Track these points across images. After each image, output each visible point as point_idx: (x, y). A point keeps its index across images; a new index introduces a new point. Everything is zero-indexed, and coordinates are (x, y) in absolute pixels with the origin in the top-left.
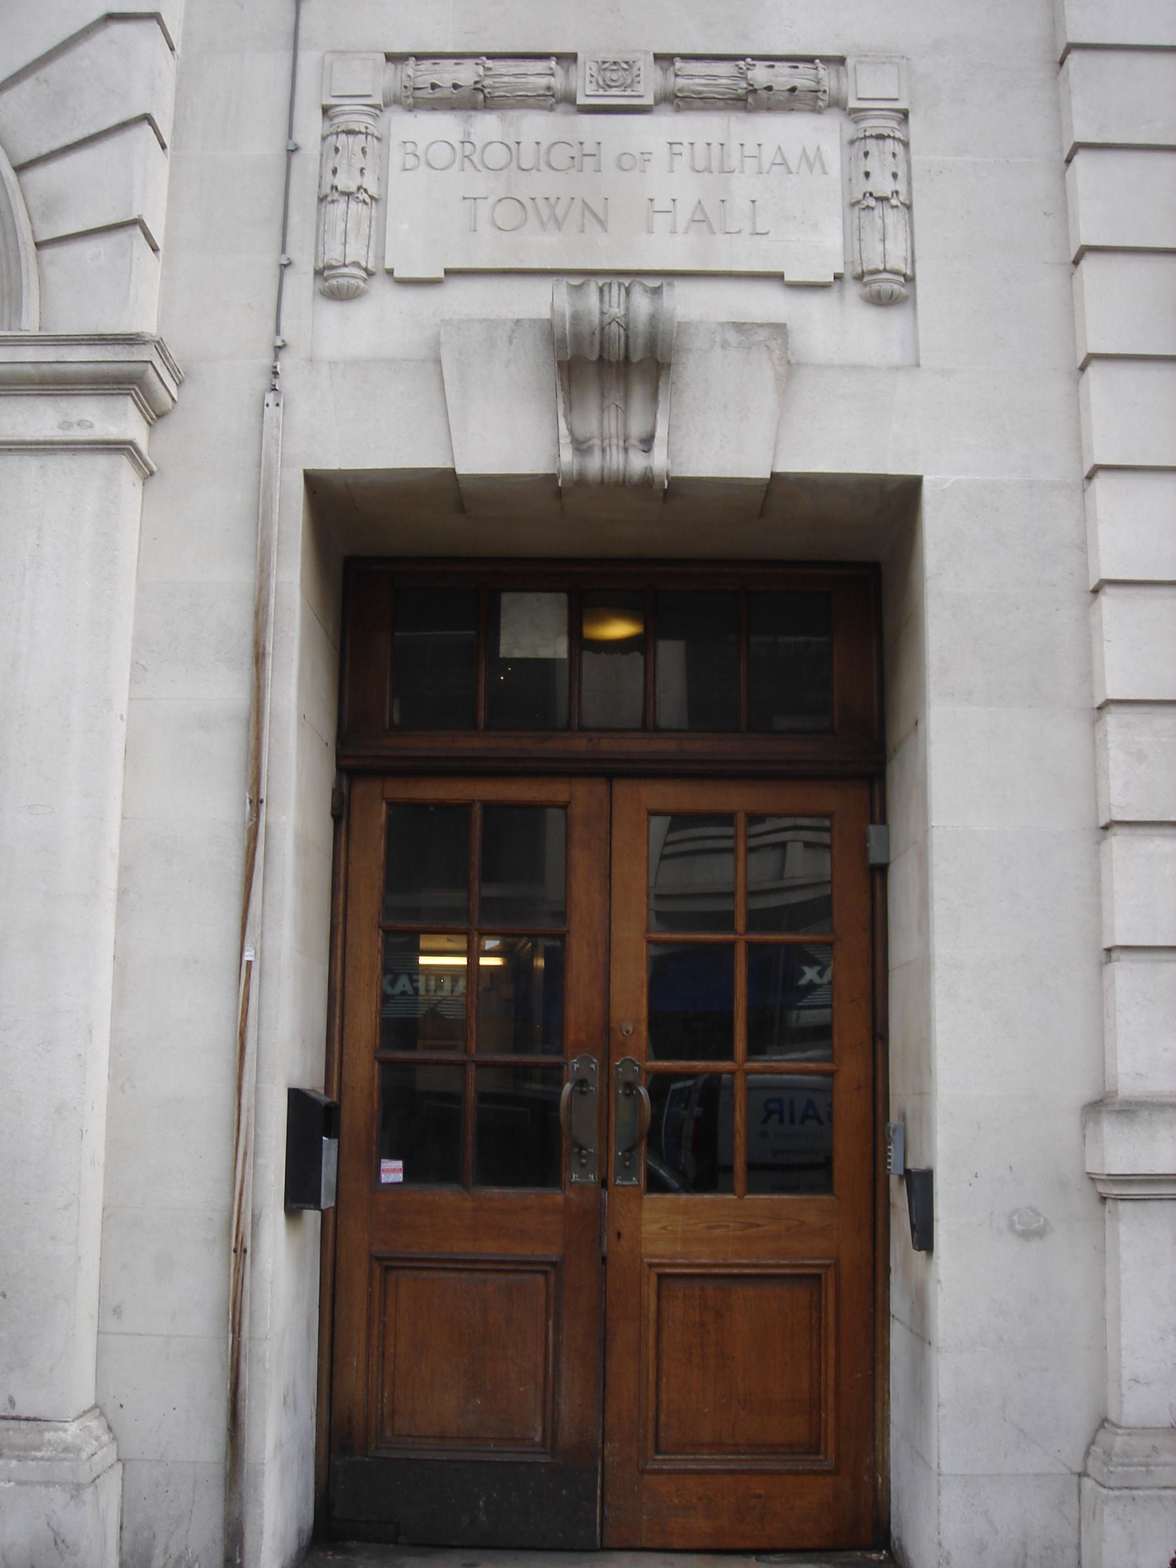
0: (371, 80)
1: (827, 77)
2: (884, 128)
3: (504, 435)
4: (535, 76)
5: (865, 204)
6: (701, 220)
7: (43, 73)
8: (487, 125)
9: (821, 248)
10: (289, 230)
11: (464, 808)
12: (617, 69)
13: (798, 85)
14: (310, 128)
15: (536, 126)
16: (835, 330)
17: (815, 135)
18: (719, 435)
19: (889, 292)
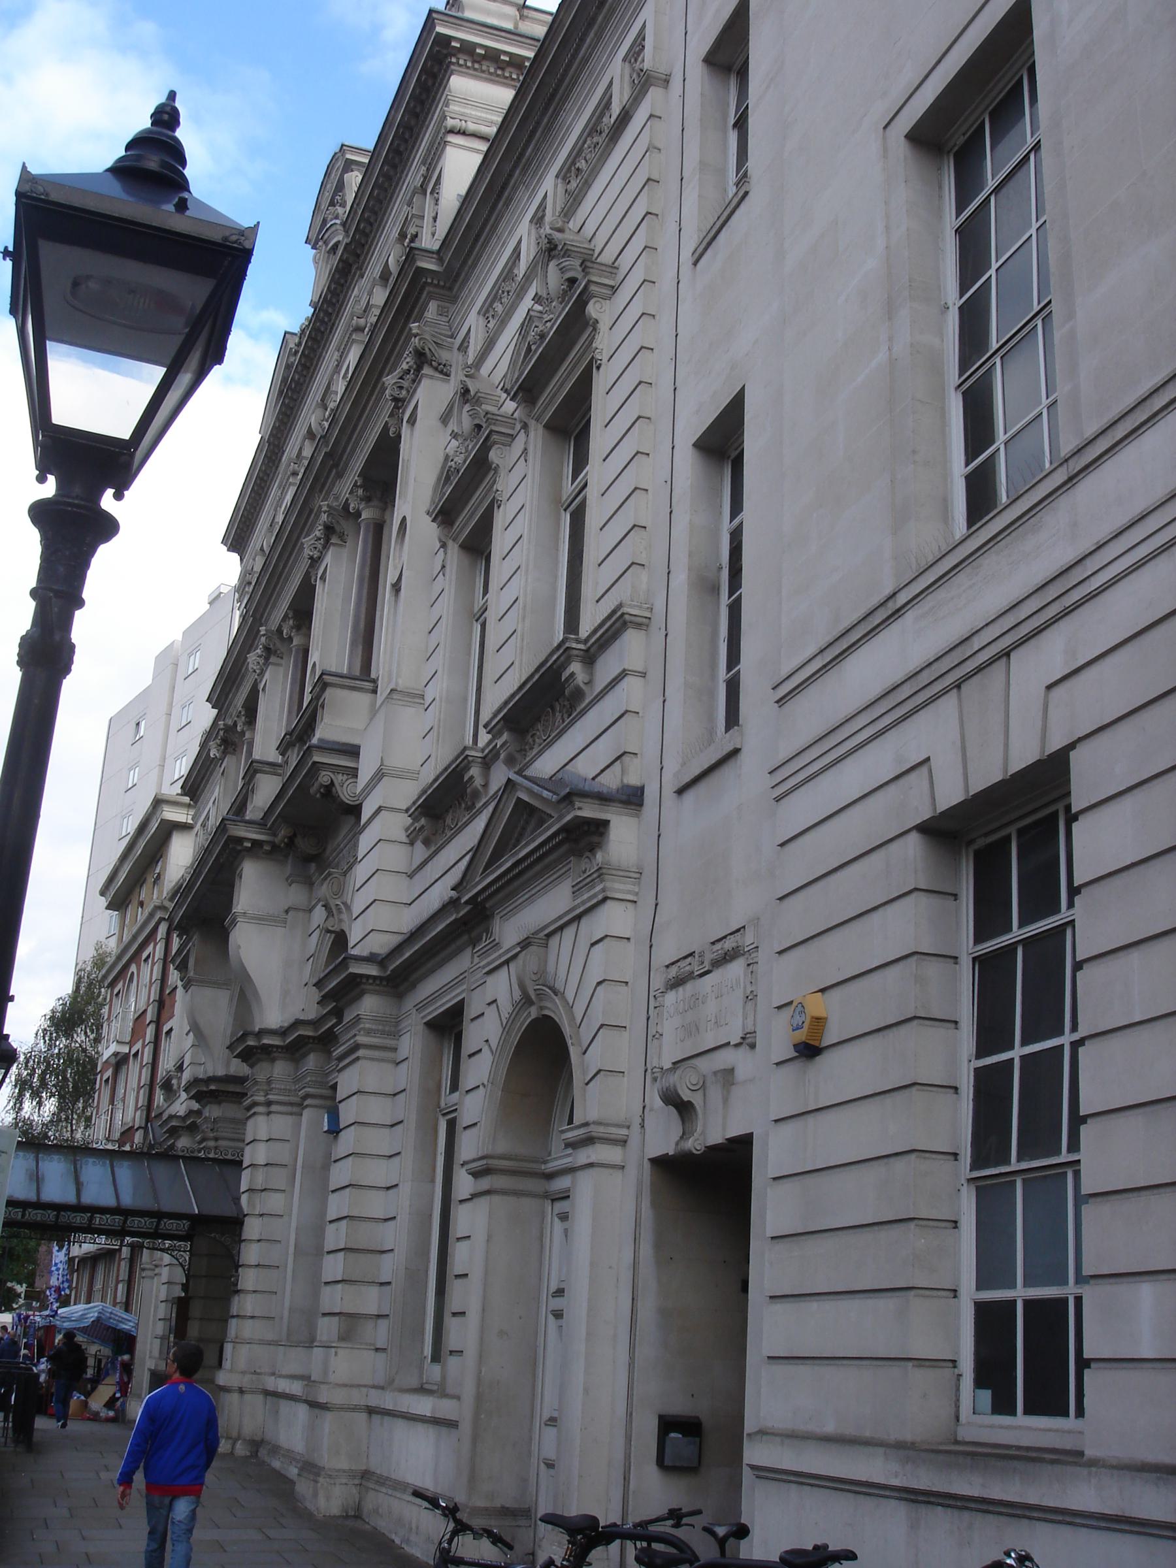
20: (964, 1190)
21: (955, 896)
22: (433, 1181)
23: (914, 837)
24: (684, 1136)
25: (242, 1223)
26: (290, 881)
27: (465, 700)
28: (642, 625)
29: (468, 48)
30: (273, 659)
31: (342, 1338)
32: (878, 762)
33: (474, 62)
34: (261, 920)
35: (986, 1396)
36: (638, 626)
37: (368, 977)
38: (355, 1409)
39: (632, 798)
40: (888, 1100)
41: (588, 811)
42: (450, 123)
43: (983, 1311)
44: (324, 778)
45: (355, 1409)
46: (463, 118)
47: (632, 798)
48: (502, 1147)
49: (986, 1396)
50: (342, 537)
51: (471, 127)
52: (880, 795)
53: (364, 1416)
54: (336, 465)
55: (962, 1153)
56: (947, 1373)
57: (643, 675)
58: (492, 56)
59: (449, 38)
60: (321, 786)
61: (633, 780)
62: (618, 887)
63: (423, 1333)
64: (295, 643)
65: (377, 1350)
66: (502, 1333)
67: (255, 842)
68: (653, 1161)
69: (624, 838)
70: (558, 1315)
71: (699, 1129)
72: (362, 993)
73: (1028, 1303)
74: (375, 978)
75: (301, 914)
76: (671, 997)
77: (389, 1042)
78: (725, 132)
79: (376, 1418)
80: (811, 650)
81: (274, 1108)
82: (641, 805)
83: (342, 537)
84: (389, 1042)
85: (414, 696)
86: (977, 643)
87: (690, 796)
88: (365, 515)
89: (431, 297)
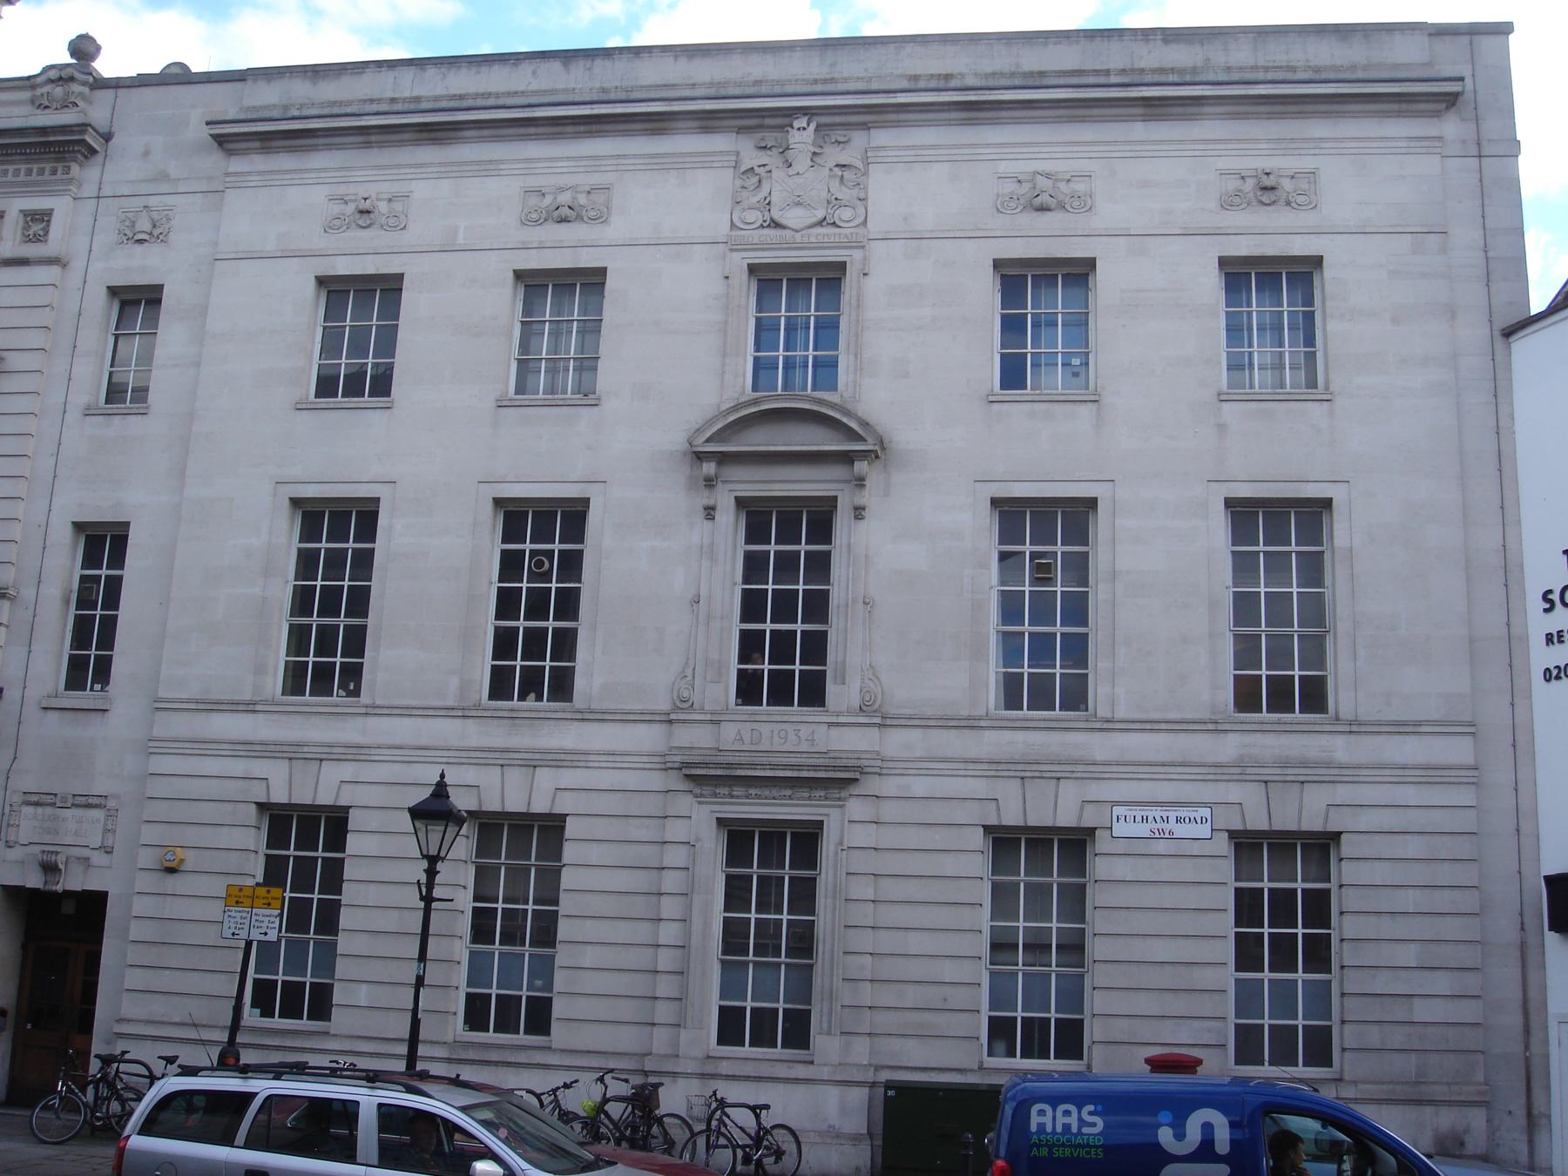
0: (18, 798)
1: (102, 801)
2: (112, 814)
3: (34, 880)
4: (48, 799)
5: (106, 831)
6: (76, 834)
7: (1465, 1110)
8: (40, 810)
9: (96, 841)
10: (789, 1086)
11: (248, 1145)
12: (64, 799)
13: (86, 802)
14: (7, 809)
15: (49, 810)
16: (98, 858)
17: (98, 814)
18: (74, 881)
19: (109, 851)
28: (12, 599)
32: (238, 767)
76: (28, 810)
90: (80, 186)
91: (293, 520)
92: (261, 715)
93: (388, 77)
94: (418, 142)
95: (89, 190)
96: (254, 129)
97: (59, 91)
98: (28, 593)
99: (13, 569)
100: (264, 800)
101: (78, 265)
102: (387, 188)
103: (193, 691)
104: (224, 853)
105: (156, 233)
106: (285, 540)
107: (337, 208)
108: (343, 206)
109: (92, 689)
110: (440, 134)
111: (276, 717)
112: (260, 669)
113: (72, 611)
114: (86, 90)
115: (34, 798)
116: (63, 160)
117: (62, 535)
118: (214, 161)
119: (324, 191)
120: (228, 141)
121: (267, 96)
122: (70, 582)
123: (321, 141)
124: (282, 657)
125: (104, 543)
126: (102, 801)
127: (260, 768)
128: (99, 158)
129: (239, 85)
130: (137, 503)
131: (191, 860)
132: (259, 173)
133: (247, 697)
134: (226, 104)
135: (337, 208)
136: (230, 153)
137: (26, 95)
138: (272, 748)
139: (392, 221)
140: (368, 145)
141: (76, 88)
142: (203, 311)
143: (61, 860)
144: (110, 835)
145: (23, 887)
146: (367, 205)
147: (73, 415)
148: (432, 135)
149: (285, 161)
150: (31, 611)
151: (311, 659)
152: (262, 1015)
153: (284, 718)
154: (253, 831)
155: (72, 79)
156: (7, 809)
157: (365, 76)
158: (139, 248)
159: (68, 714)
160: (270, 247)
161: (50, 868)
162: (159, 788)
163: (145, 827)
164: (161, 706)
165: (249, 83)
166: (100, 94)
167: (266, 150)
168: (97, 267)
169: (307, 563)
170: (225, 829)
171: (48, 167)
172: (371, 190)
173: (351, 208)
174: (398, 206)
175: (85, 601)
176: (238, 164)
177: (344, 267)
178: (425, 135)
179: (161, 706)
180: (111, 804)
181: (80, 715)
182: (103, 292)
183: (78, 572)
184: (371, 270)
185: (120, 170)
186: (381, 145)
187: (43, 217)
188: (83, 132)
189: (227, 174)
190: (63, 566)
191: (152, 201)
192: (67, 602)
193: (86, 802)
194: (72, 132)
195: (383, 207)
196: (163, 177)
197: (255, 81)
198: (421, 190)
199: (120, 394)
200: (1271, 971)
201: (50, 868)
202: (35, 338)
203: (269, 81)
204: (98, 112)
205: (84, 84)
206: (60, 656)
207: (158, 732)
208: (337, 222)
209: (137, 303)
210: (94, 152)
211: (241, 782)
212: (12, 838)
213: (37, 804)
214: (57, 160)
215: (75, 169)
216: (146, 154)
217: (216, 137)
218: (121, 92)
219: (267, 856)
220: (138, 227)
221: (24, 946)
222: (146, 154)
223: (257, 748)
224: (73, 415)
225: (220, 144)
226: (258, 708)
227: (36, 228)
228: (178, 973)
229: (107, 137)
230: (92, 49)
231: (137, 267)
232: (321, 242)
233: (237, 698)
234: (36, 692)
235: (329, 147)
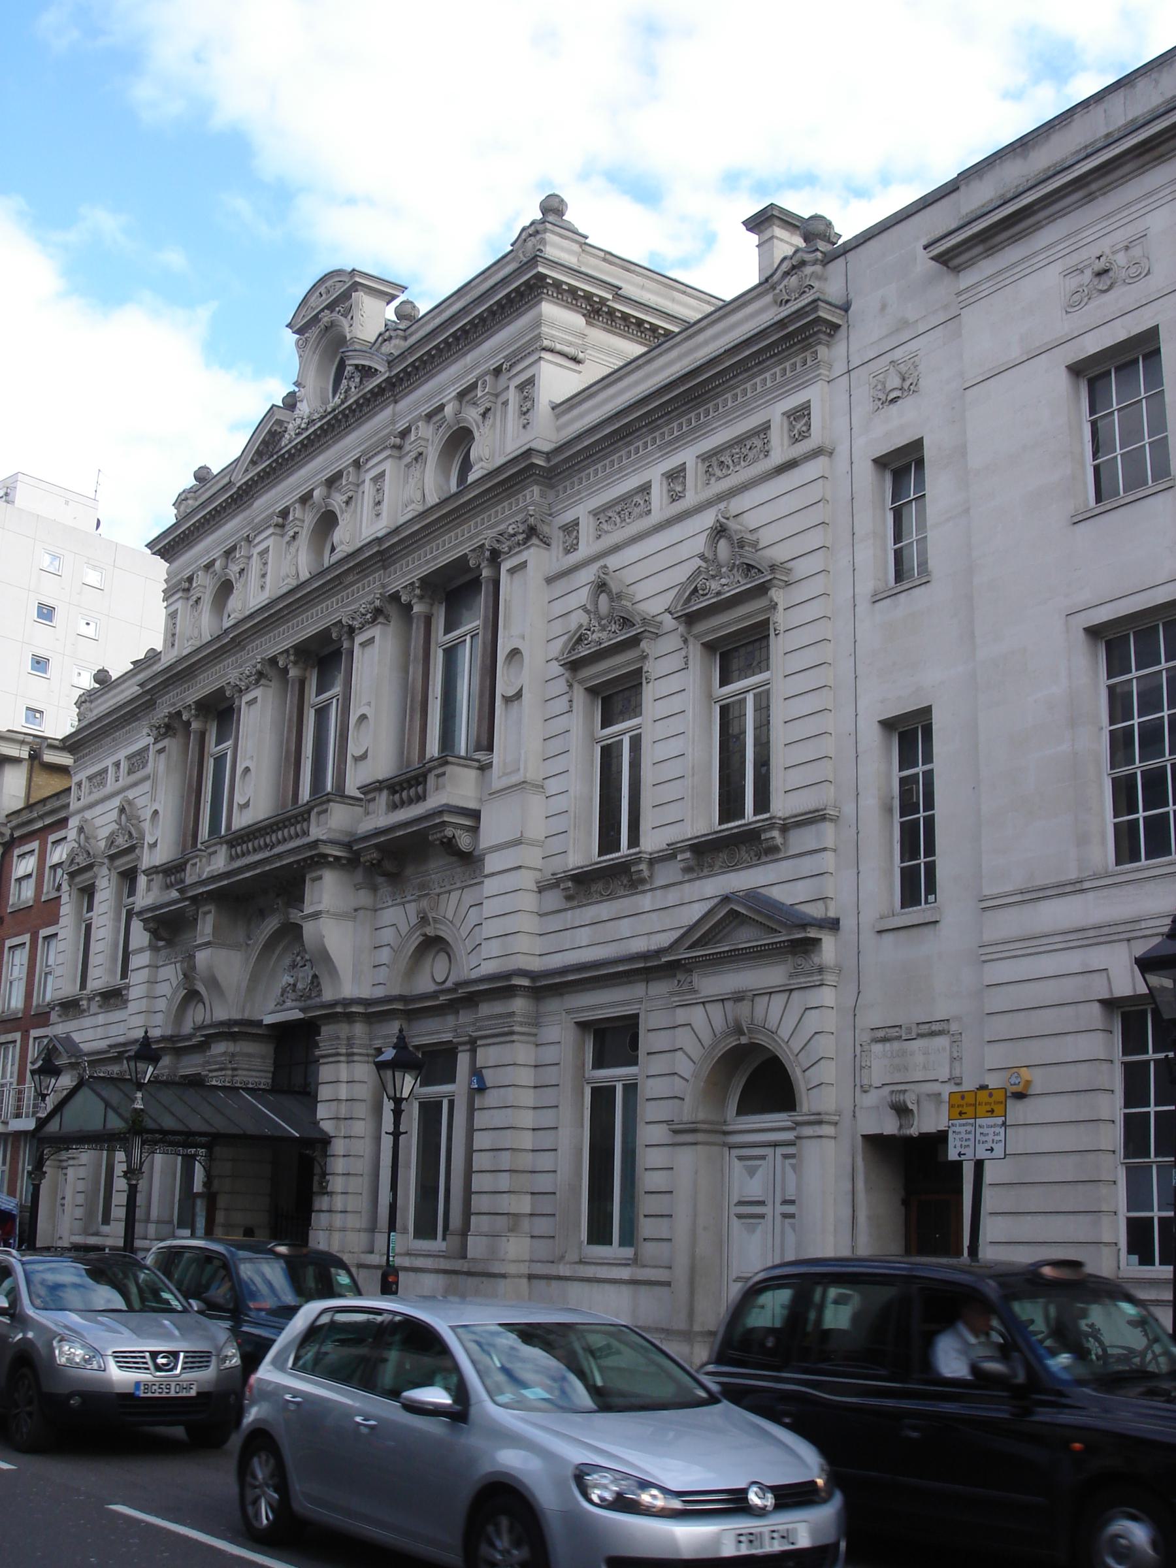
0: (866, 1037)
1: (944, 1026)
3: (889, 1126)
4: (893, 1033)
9: (944, 1074)
12: (909, 1030)
13: (931, 1030)
14: (858, 1049)
15: (896, 1045)
17: (942, 1042)
20: (1119, 1167)
21: (1111, 1032)
22: (582, 1126)
23: (1097, 1005)
24: (901, 1127)
25: (329, 1142)
26: (357, 887)
27: (591, 799)
28: (835, 820)
29: (557, 284)
30: (263, 681)
31: (510, 1230)
32: (1073, 961)
33: (558, 293)
34: (339, 916)
35: (1135, 1258)
36: (831, 820)
37: (521, 986)
38: (520, 1276)
39: (833, 925)
40: (1082, 1126)
41: (812, 933)
42: (546, 343)
43: (1131, 1222)
44: (449, 832)
45: (520, 1276)
46: (552, 338)
47: (833, 925)
48: (701, 1116)
49: (1135, 1258)
50: (387, 618)
51: (559, 347)
52: (1070, 978)
53: (525, 1281)
54: (384, 561)
55: (1118, 1150)
56: (1114, 1248)
57: (835, 851)
58: (573, 291)
59: (546, 276)
60: (445, 837)
61: (832, 914)
62: (830, 978)
63: (579, 1226)
64: (291, 674)
65: (532, 1237)
66: (705, 1228)
67: (337, 858)
68: (866, 1137)
69: (829, 949)
70: (63, 1205)
71: (916, 1123)
72: (515, 996)
73: (1160, 1218)
74: (525, 987)
75: (369, 912)
76: (877, 1048)
77: (534, 1031)
78: (884, 509)
79: (535, 1282)
80: (1009, 888)
81: (356, 1058)
82: (838, 929)
83: (387, 618)
84: (534, 1031)
85: (537, 786)
86: (1143, 925)
87: (888, 938)
88: (416, 609)
89: (537, 483)
90: (830, 367)
91: (1095, 656)
92: (1090, 896)
93: (1097, 112)
94: (1142, 170)
95: (839, 368)
96: (970, 233)
97: (793, 281)
98: (848, 809)
99: (832, 788)
100: (1107, 996)
101: (842, 450)
102: (1121, 236)
103: (1017, 881)
104: (1072, 1067)
105: (908, 383)
106: (1084, 680)
107: (1073, 282)
108: (1080, 278)
109: (926, 902)
110: (1162, 149)
111: (1105, 892)
112: (1082, 840)
113: (897, 819)
114: (818, 268)
115: (881, 1034)
116: (808, 347)
117: (871, 736)
118: (948, 286)
119: (1058, 267)
120: (951, 258)
121: (982, 194)
122: (891, 791)
123: (1042, 215)
124: (1110, 820)
125: (910, 733)
126: (944, 1026)
127: (1097, 957)
128: (843, 330)
129: (954, 195)
130: (934, 683)
131: (1039, 1081)
132: (989, 278)
133: (1073, 876)
134: (940, 220)
135: (1073, 282)
136: (957, 270)
137: (768, 298)
138: (1106, 931)
139: (1132, 271)
140: (1090, 198)
141: (808, 270)
142: (962, 451)
143: (910, 1101)
144: (957, 1064)
145: (882, 1135)
146: (1100, 265)
147: (863, 607)
148: (1156, 153)
149: (1012, 254)
150: (854, 830)
151: (1141, 815)
152: (1141, 1263)
153: (1114, 891)
154: (1100, 1035)
155: (803, 263)
156: (858, 1049)
157: (1074, 125)
158: (894, 408)
159: (902, 933)
160: (1016, 354)
161: (902, 1111)
162: (998, 1000)
163: (988, 1049)
164: (989, 905)
165: (963, 189)
166: (831, 266)
167: (990, 252)
168: (860, 442)
169: (1118, 704)
170: (1069, 1038)
171: (798, 359)
172: (1104, 246)
173: (1088, 273)
174: (1136, 252)
175: (908, 806)
176: (968, 278)
177: (1093, 345)
178: (1147, 157)
179: (989, 905)
180: (954, 1027)
181: (914, 931)
182: (869, 465)
183: (896, 775)
184: (1122, 336)
185: (864, 336)
186: (1104, 191)
187: (801, 413)
188: (816, 309)
189: (958, 294)
190: (878, 770)
191: (898, 354)
192: (890, 810)
193: (931, 1030)
194: (807, 314)
195: (1121, 259)
196: (904, 324)
197: (967, 184)
198: (1158, 221)
199: (904, 570)
200: (1168, 805)
201: (902, 1111)
202: (814, 539)
203: (981, 178)
204: (832, 287)
205: (815, 262)
206: (890, 872)
207: (987, 937)
208: (1077, 297)
209: (903, 466)
210: (836, 327)
211: (1080, 978)
212: (865, 1082)
213: (884, 1040)
214: (804, 349)
215: (822, 351)
216: (884, 307)
217: (939, 259)
218: (850, 255)
219: (1125, 1064)
220: (889, 387)
221: (905, 1202)
222: (884, 307)
223: (1091, 933)
224: (863, 607)
225: (945, 263)
226: (1087, 885)
227: (799, 426)
228: (1040, 1218)
229: (846, 308)
230: (822, 227)
231: (891, 430)
232: (1064, 326)
233: (1063, 878)
234: (870, 916)
235: (1052, 219)
